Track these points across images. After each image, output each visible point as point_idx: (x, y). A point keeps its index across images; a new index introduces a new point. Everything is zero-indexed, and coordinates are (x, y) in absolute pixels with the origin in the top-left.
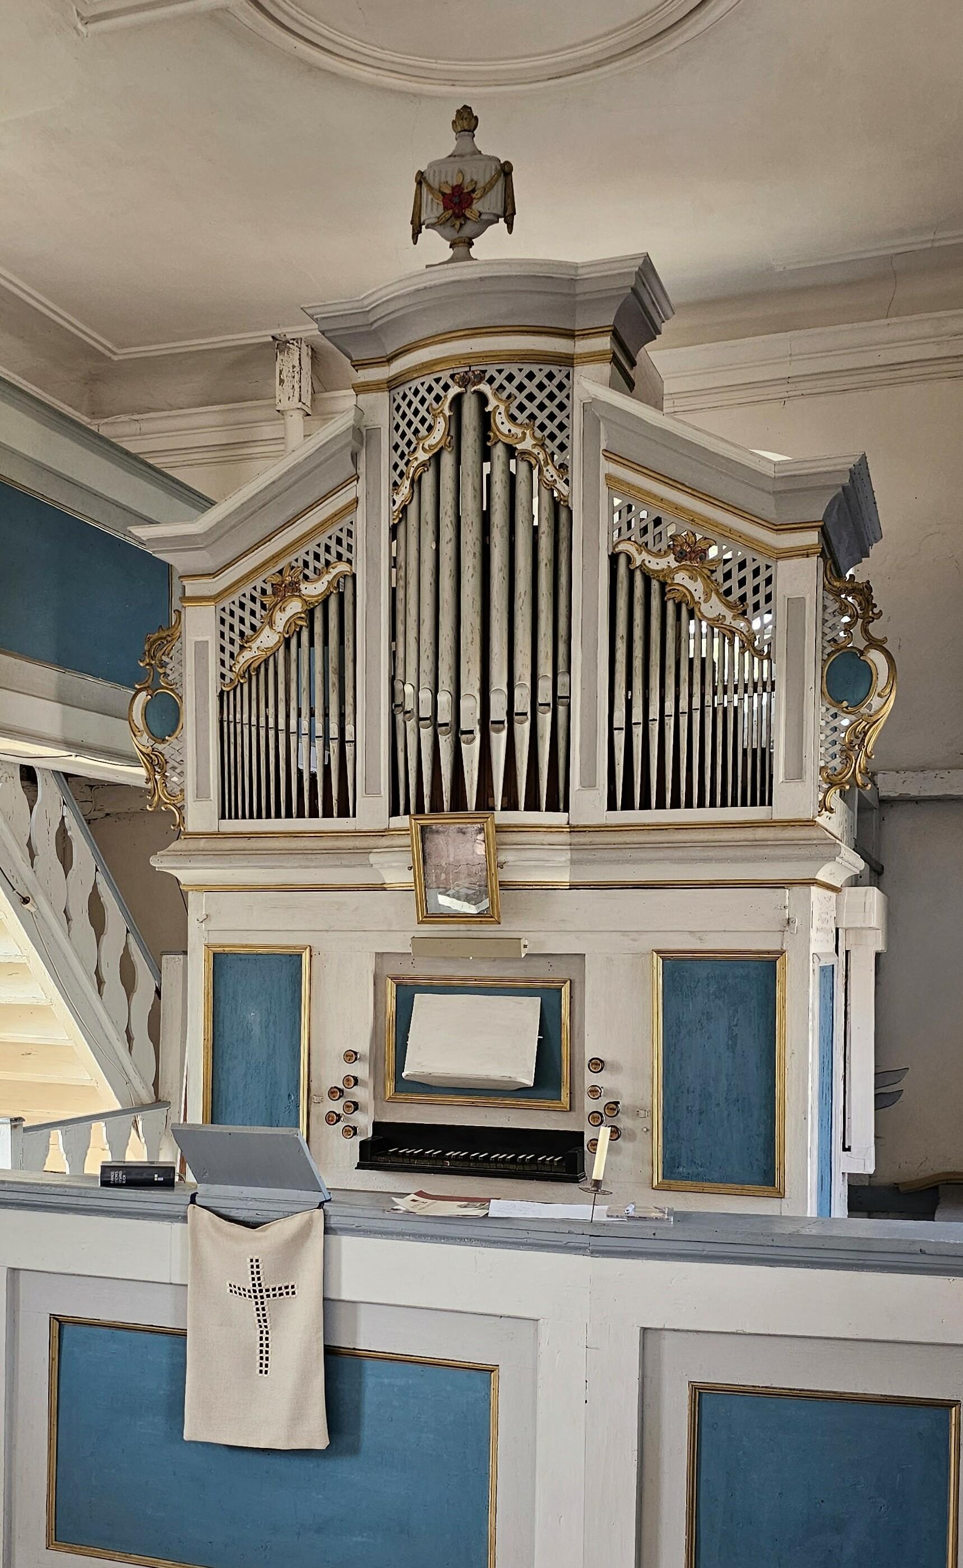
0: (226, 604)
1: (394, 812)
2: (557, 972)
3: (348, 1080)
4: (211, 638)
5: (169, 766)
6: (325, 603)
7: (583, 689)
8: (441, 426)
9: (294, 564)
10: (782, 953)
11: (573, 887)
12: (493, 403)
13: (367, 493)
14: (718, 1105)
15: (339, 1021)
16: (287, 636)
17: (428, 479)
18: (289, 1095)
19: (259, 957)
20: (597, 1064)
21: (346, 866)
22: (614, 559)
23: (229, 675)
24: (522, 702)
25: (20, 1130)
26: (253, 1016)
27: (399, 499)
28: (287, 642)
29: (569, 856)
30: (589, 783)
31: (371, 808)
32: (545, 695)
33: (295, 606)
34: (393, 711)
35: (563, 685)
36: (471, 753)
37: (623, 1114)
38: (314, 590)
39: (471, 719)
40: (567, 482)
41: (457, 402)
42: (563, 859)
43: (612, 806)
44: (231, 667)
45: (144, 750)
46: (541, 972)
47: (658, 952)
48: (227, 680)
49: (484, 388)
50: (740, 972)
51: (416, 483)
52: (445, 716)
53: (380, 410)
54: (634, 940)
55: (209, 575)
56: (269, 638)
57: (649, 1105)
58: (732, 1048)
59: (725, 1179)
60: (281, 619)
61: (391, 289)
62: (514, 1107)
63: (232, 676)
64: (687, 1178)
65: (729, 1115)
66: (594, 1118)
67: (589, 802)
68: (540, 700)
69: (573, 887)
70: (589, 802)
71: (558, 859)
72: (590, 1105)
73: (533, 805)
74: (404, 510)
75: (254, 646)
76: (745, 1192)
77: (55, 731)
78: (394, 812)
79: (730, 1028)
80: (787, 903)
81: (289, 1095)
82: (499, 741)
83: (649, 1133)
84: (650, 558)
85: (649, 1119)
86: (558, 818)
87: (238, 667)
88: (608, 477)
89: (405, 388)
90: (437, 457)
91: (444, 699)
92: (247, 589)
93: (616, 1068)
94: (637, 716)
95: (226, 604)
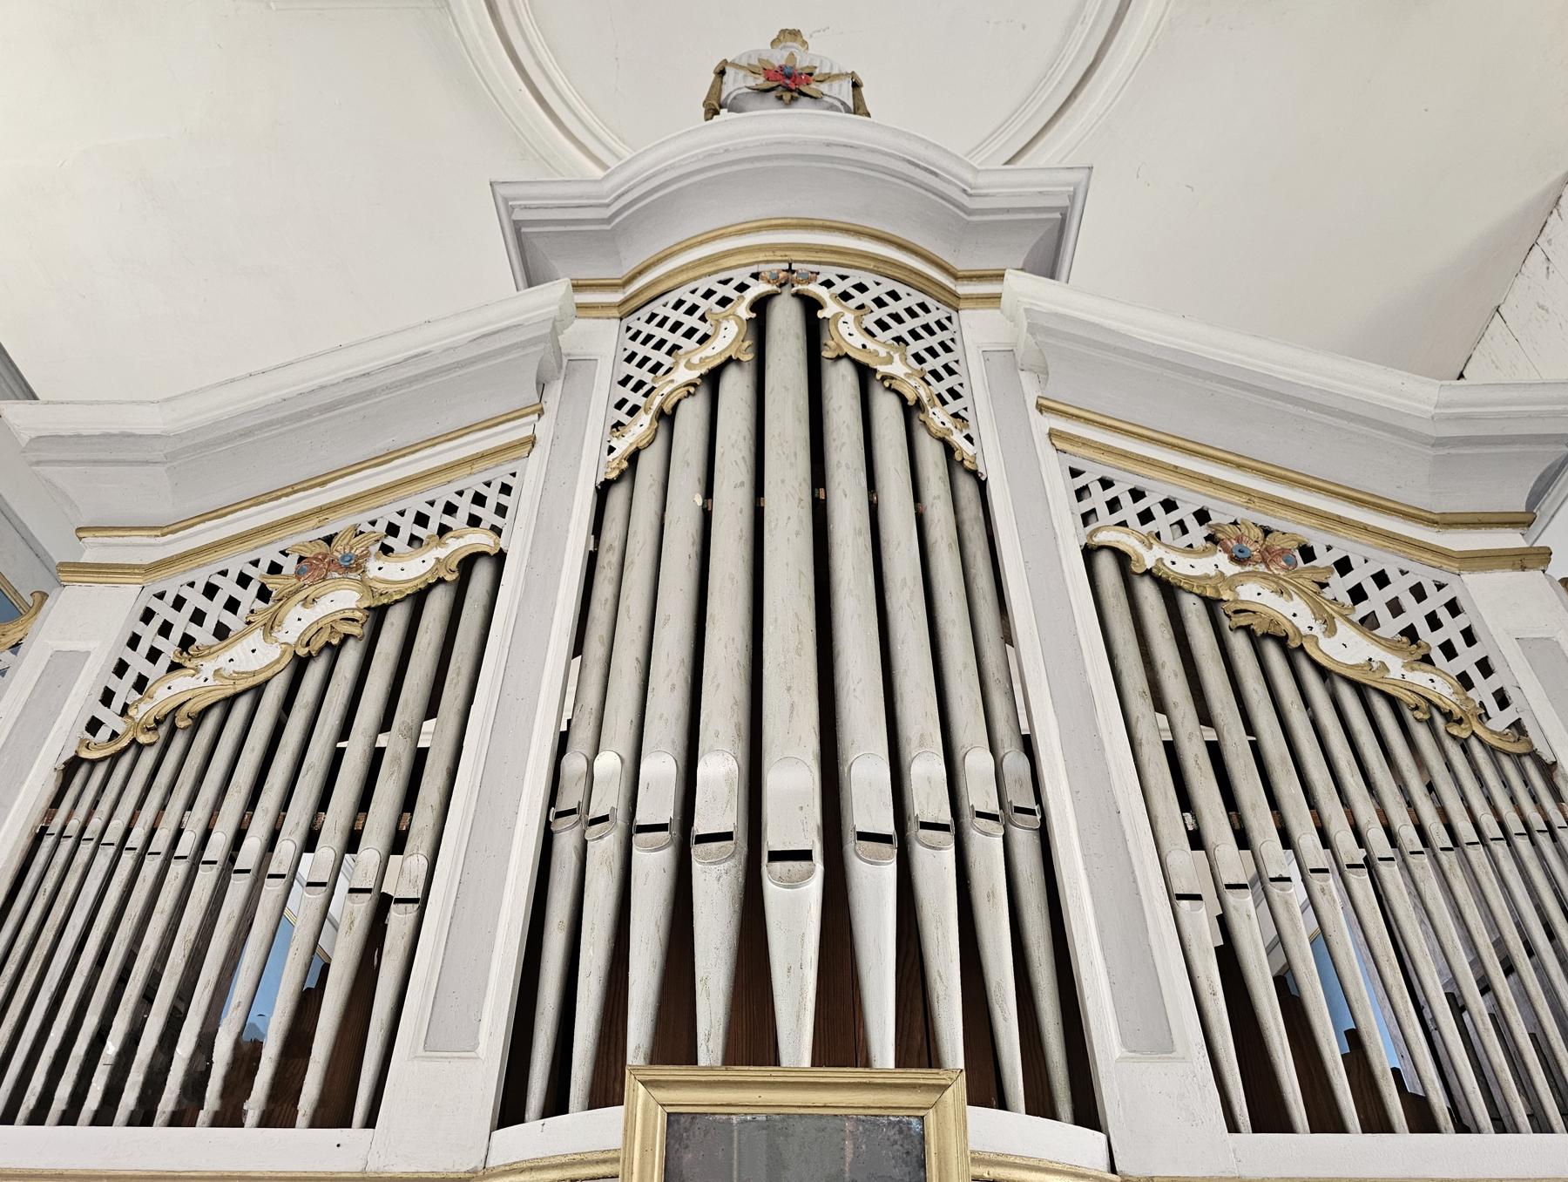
1: (510, 1112)
4: (104, 647)
6: (418, 600)
7: (1075, 793)
8: (728, 336)
9: (367, 528)
12: (830, 310)
13: (555, 438)
16: (302, 652)
17: (691, 416)
22: (1089, 553)
24: (928, 801)
27: (623, 446)
28: (300, 666)
31: (440, 1075)
33: (342, 599)
34: (548, 824)
35: (1019, 781)
36: (794, 909)
38: (405, 570)
39: (793, 817)
40: (969, 438)
41: (761, 306)
43: (1233, 1127)
44: (126, 706)
49: (822, 293)
51: (667, 418)
52: (718, 808)
53: (602, 343)
56: (255, 654)
60: (297, 623)
61: (663, 151)
63: (120, 725)
67: (1163, 1078)
73: (986, 1088)
74: (634, 458)
75: (208, 667)
78: (510, 1112)
82: (874, 882)
84: (1173, 556)
87: (144, 708)
88: (1052, 434)
89: (656, 307)
90: (713, 379)
91: (720, 768)
92: (237, 563)
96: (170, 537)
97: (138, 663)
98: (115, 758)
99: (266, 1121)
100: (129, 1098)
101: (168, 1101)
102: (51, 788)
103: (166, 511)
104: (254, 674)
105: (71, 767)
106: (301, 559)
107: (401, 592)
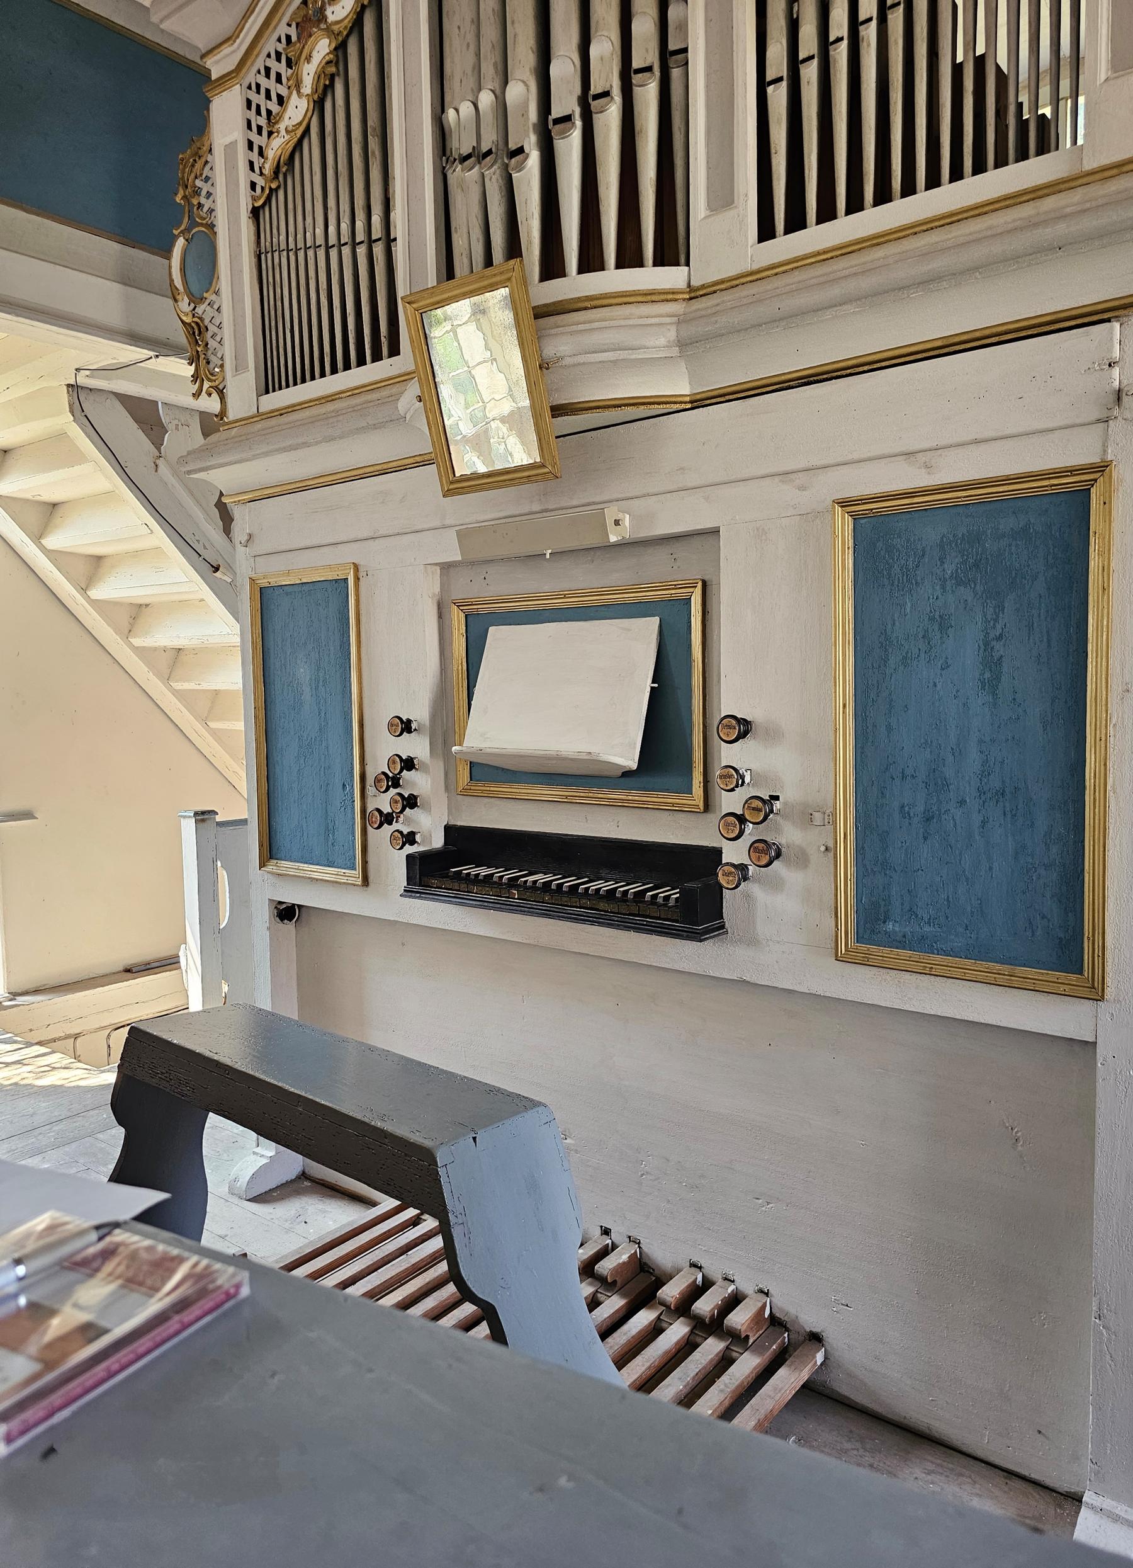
0: (251, 77)
1: (766, 232)
2: (683, 567)
3: (394, 762)
5: (210, 334)
7: (708, 20)
10: (1102, 468)
11: (698, 403)
14: (962, 803)
15: (398, 666)
18: (344, 785)
19: (305, 588)
20: (730, 727)
21: (375, 427)
23: (260, 182)
24: (605, 75)
25: (209, 826)
26: (303, 672)
29: (672, 334)
30: (722, 199)
32: (645, 53)
37: (786, 817)
42: (662, 341)
45: (184, 318)
46: (658, 573)
47: (844, 503)
48: (258, 189)
50: (1008, 523)
54: (802, 488)
55: (229, 39)
56: (297, 110)
57: (831, 803)
58: (991, 684)
59: (979, 952)
60: (309, 72)
62: (623, 805)
64: (901, 943)
65: (984, 823)
66: (727, 825)
68: (636, 64)
69: (698, 403)
70: (723, 233)
71: (651, 342)
72: (731, 802)
76: (1015, 981)
77: (114, 317)
79: (986, 644)
80: (1116, 354)
81: (344, 785)
83: (831, 854)
85: (830, 827)
86: (672, 277)
93: (773, 735)
94: (808, 43)
95: (251, 77)
96: (238, 41)
97: (257, 140)
98: (269, 199)
99: (877, 202)
100: (277, 386)
101: (340, 365)
102: (252, 229)
103: (227, 24)
104: (300, 124)
105: (255, 213)
106: (297, 24)
107: (346, 27)
